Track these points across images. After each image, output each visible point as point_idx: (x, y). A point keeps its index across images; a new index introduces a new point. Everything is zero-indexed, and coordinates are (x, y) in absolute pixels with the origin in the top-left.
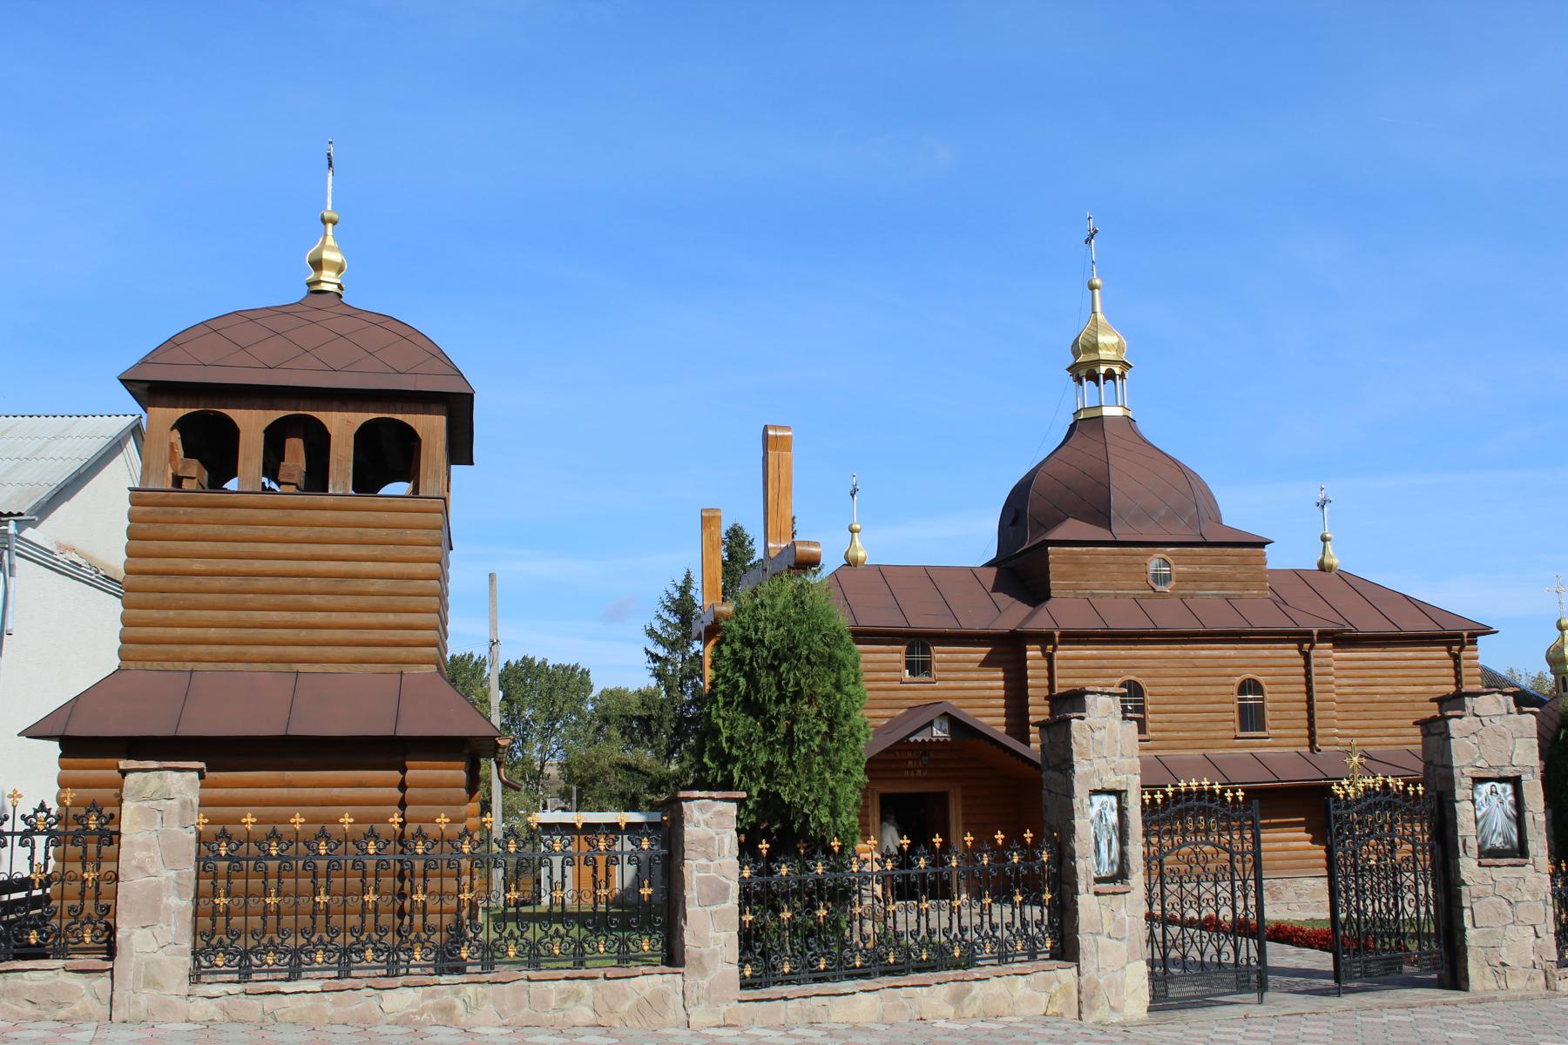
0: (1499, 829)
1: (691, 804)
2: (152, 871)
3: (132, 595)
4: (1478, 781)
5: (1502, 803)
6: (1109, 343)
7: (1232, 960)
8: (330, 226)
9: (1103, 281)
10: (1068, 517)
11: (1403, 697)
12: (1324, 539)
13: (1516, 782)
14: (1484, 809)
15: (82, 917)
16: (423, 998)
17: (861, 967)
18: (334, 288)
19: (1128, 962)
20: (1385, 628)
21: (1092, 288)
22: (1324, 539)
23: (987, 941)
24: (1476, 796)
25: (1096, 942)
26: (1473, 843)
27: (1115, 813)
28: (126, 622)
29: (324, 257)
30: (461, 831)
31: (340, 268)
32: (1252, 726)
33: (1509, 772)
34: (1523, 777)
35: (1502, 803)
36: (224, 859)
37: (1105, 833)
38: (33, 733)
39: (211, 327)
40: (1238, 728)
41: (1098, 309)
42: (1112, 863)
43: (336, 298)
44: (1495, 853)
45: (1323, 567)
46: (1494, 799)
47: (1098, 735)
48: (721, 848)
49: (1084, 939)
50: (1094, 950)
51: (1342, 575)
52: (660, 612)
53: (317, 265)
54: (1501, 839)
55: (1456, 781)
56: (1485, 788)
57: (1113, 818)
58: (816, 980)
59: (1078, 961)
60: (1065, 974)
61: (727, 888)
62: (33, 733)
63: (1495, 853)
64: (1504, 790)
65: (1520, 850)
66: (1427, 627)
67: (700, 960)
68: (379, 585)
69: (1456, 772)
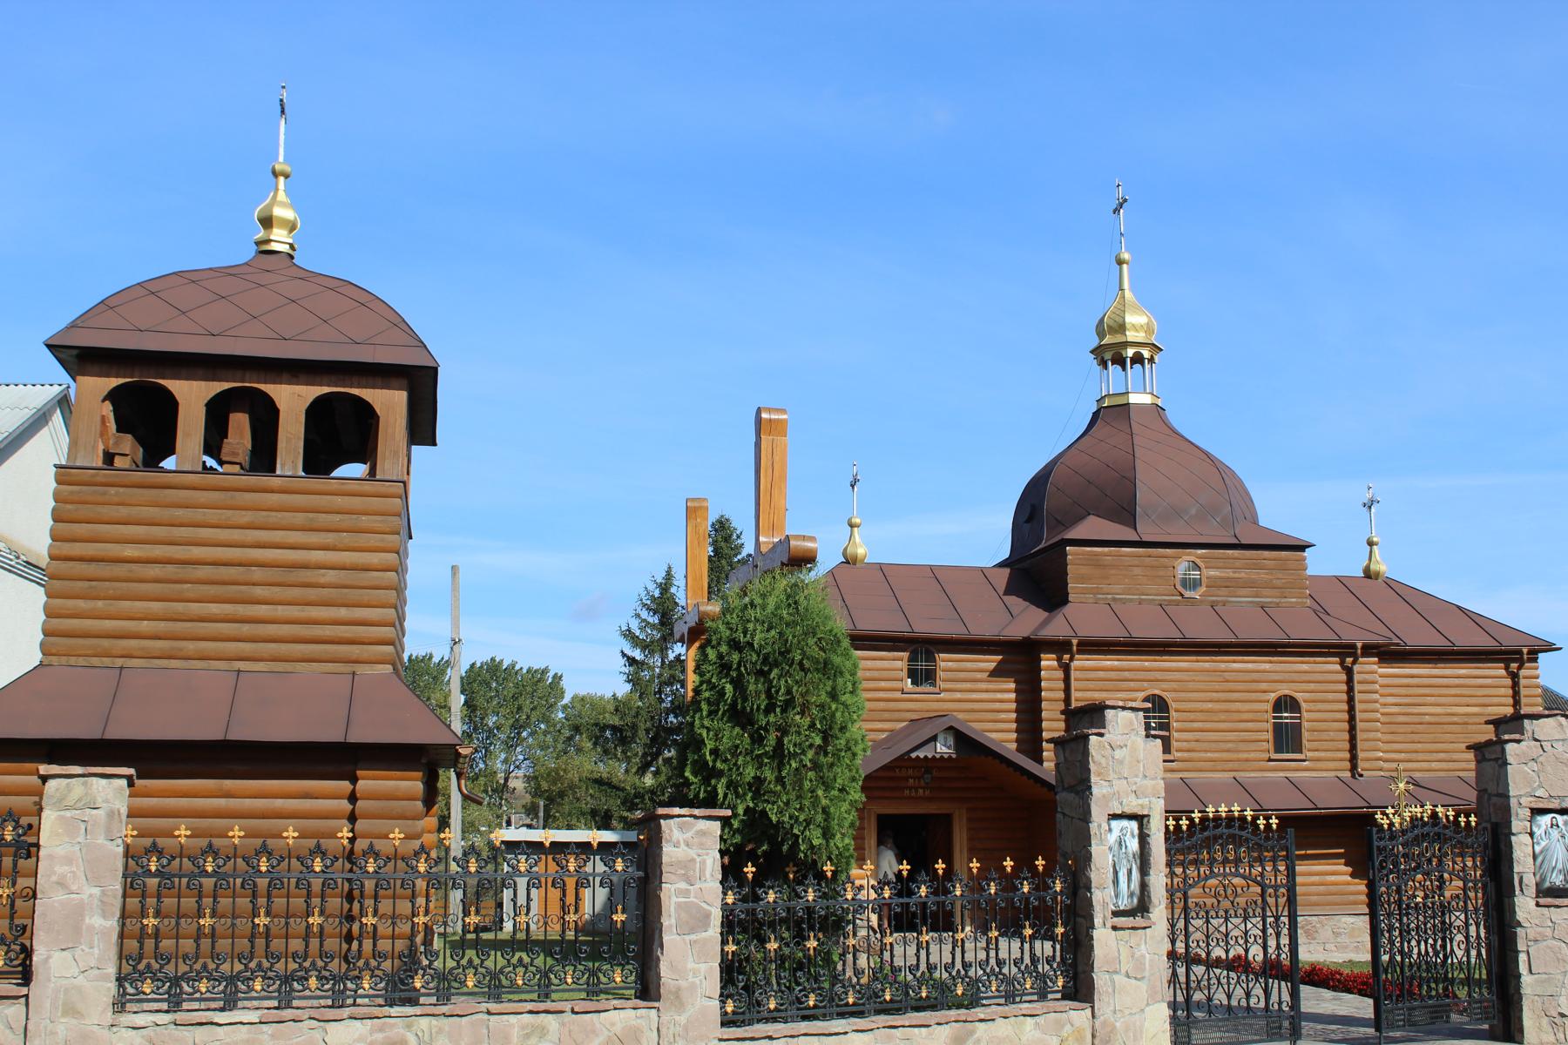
0: (1560, 866)
1: (671, 822)
2: (74, 888)
4: (1537, 812)
6: (1137, 323)
7: (1262, 1004)
11: (1455, 719)
12: (1371, 544)
14: (1543, 844)
16: (372, 1032)
17: (854, 1004)
18: (285, 248)
19: (1148, 1005)
21: (1120, 262)
22: (1371, 544)
24: (1535, 829)
25: (1113, 981)
26: (1530, 880)
27: (1136, 840)
30: (417, 848)
31: (292, 227)
36: (154, 875)
37: (1125, 862)
40: (1272, 749)
41: (1126, 285)
42: (1131, 895)
45: (1368, 574)
46: (1555, 833)
48: (702, 871)
49: (1100, 978)
50: (1110, 990)
51: (1390, 584)
52: (639, 611)
53: (267, 222)
54: (1561, 877)
55: (1513, 811)
56: (1545, 820)
57: (1133, 845)
60: (1079, 1016)
61: (708, 915)
67: (677, 994)
68: (331, 577)
69: (1513, 802)
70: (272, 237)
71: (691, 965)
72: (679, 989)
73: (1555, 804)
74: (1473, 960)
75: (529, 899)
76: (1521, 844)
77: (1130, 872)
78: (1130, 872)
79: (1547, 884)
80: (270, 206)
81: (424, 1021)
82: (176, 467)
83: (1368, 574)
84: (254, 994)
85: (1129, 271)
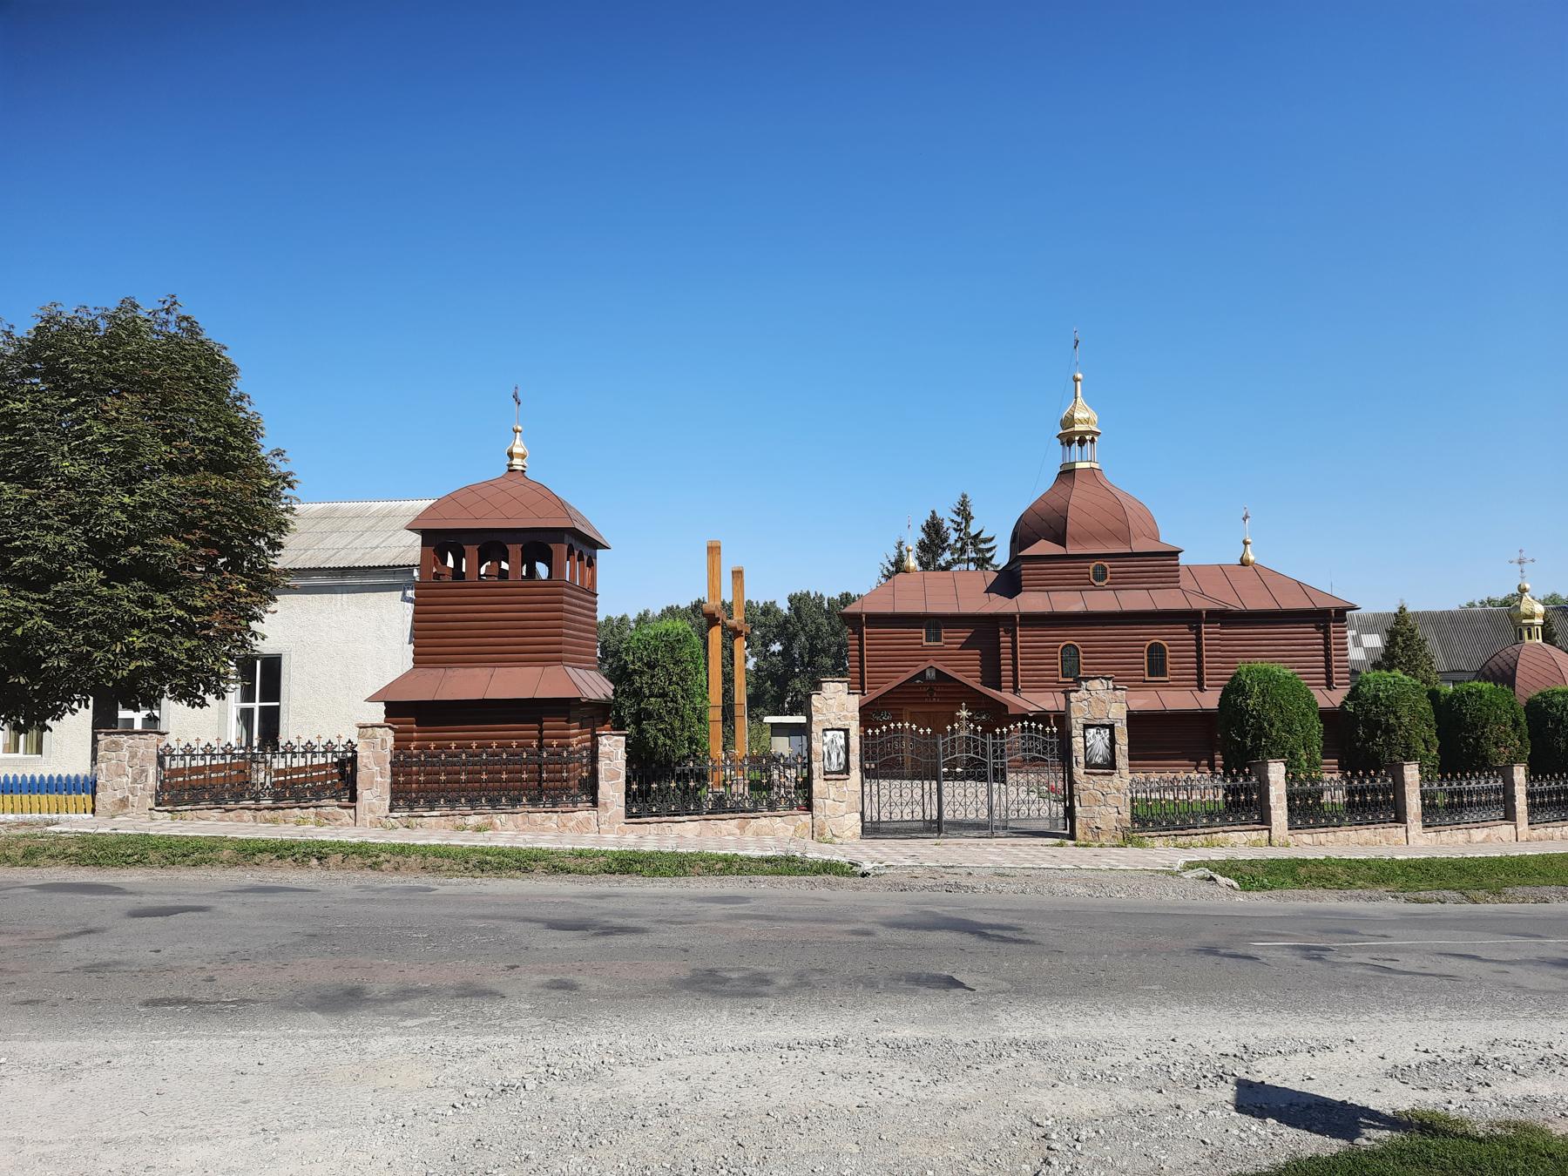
0: (1101, 753)
1: (603, 737)
3: (592, 614)
4: (1086, 727)
5: (1103, 738)
6: (1085, 416)
7: (1047, 814)
8: (518, 433)
12: (1245, 543)
13: (1111, 727)
14: (1091, 742)
15: (265, 787)
16: (484, 819)
17: (675, 811)
18: (520, 468)
20: (1267, 604)
21: (1076, 380)
22: (1245, 543)
23: (783, 799)
24: (1087, 734)
25: (824, 802)
26: (1081, 759)
27: (843, 740)
28: (415, 653)
29: (514, 451)
31: (523, 456)
33: (1106, 722)
34: (1116, 725)
35: (1103, 738)
39: (452, 497)
40: (1146, 674)
41: (1079, 394)
43: (521, 474)
45: (1244, 563)
46: (1098, 737)
47: (829, 702)
49: (816, 801)
51: (1257, 569)
52: (880, 578)
53: (511, 455)
54: (1101, 759)
55: (1073, 726)
56: (1092, 731)
57: (842, 742)
60: (806, 818)
65: (1111, 764)
66: (1303, 604)
67: (605, 804)
70: (513, 463)
71: (611, 793)
72: (606, 803)
73: (1097, 722)
74: (995, 802)
75: (265, 778)
76: (1077, 742)
77: (838, 755)
78: (838, 755)
79: (1093, 762)
80: (512, 447)
81: (503, 815)
82: (143, 728)
83: (1244, 563)
84: (690, 812)
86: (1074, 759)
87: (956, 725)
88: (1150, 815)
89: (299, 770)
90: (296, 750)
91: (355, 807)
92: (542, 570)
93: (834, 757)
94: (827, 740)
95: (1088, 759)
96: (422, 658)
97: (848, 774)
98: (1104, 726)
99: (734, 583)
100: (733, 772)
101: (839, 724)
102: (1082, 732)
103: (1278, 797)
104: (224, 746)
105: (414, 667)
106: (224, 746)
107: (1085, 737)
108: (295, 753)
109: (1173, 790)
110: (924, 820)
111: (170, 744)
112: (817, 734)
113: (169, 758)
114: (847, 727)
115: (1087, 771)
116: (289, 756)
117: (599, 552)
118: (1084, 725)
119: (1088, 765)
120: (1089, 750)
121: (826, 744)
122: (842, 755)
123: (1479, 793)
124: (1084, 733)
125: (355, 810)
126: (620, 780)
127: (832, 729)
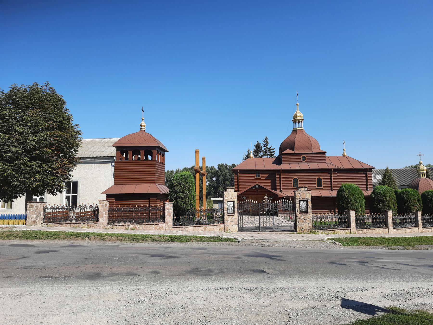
0: (304, 208)
1: (167, 204)
4: (300, 201)
7: (289, 225)
8: (143, 120)
9: (299, 103)
10: (287, 149)
12: (344, 150)
13: (307, 201)
14: (301, 205)
15: (73, 218)
16: (134, 226)
17: (186, 224)
18: (144, 129)
21: (297, 105)
22: (344, 150)
23: (216, 221)
24: (300, 203)
25: (228, 222)
26: (299, 210)
27: (233, 204)
31: (144, 126)
32: (320, 186)
33: (305, 199)
34: (308, 200)
38: (102, 193)
39: (125, 137)
41: (298, 109)
42: (232, 211)
44: (303, 212)
45: (344, 156)
46: (303, 204)
47: (229, 194)
48: (170, 209)
49: (225, 221)
51: (347, 157)
52: (243, 160)
53: (141, 126)
54: (304, 210)
55: (296, 201)
56: (302, 202)
57: (233, 205)
58: (190, 225)
59: (388, 227)
60: (223, 226)
62: (102, 193)
63: (303, 212)
64: (305, 202)
65: (307, 211)
66: (360, 167)
67: (167, 222)
69: (296, 199)
70: (142, 128)
71: (169, 219)
73: (303, 200)
75: (73, 215)
76: (297, 205)
77: (232, 209)
78: (232, 209)
79: (302, 211)
80: (141, 124)
81: (139, 225)
83: (344, 156)
84: (191, 224)
85: (299, 106)
86: (297, 210)
87: (264, 200)
88: (317, 225)
89: (83, 213)
90: (82, 207)
91: (98, 223)
92: (150, 157)
93: (230, 209)
94: (228, 204)
95: (300, 210)
96: (117, 182)
97: (234, 214)
98: (305, 201)
99: (203, 161)
100: (202, 213)
101: (232, 200)
102: (299, 202)
103: (353, 220)
104: (62, 206)
105: (114, 184)
106: (62, 206)
107: (300, 204)
108: (81, 208)
109: (324, 218)
110: (255, 227)
111: (47, 206)
112: (226, 203)
113: (63, 209)
114: (234, 201)
115: (300, 213)
116: (80, 209)
117: (165, 153)
118: (299, 200)
119: (300, 211)
120: (301, 207)
121: (228, 206)
122: (233, 209)
123: (408, 219)
124: (299, 203)
125: (98, 224)
126: (171, 216)
127: (230, 202)
